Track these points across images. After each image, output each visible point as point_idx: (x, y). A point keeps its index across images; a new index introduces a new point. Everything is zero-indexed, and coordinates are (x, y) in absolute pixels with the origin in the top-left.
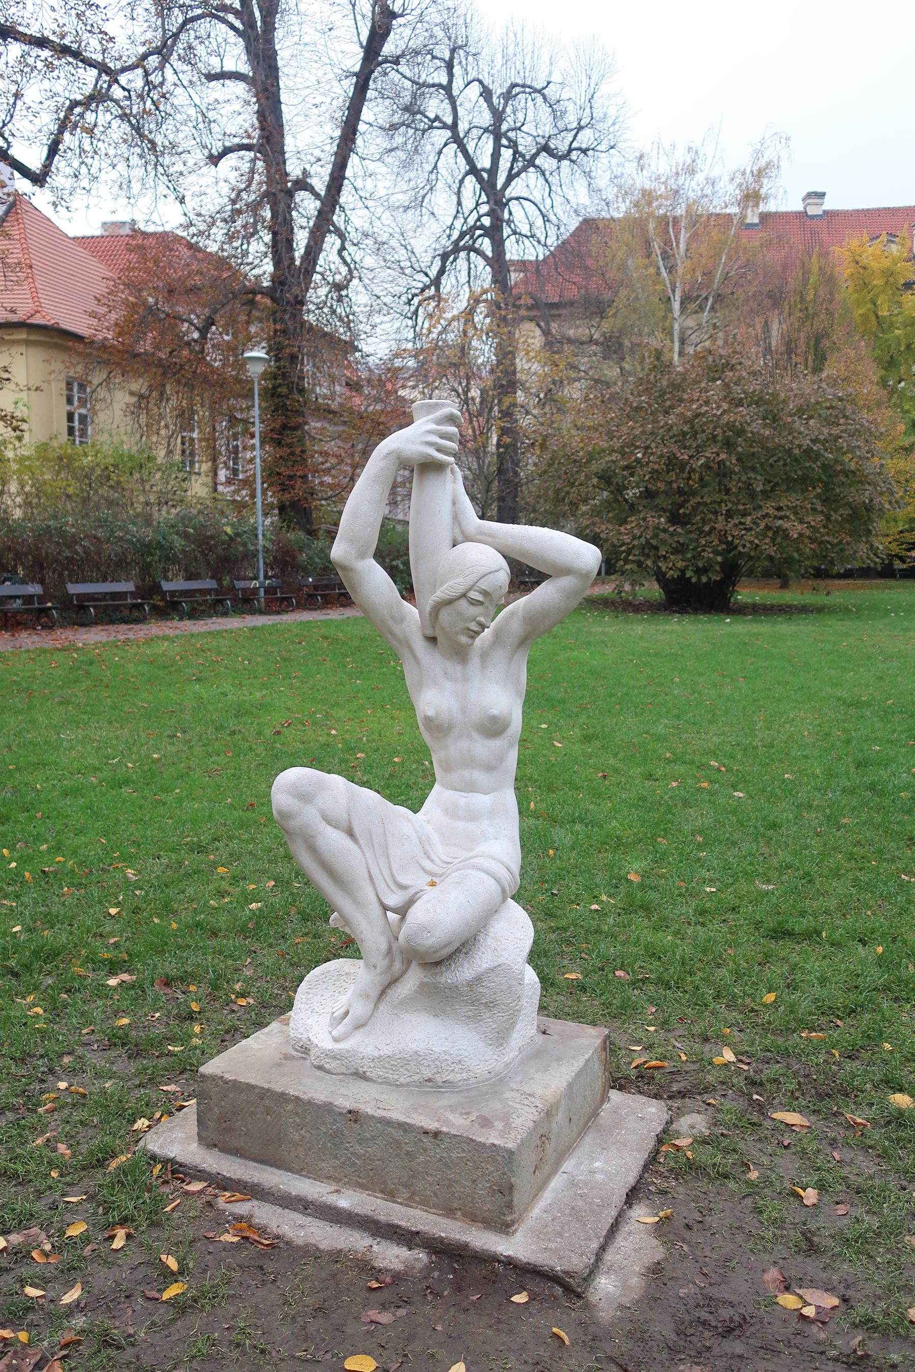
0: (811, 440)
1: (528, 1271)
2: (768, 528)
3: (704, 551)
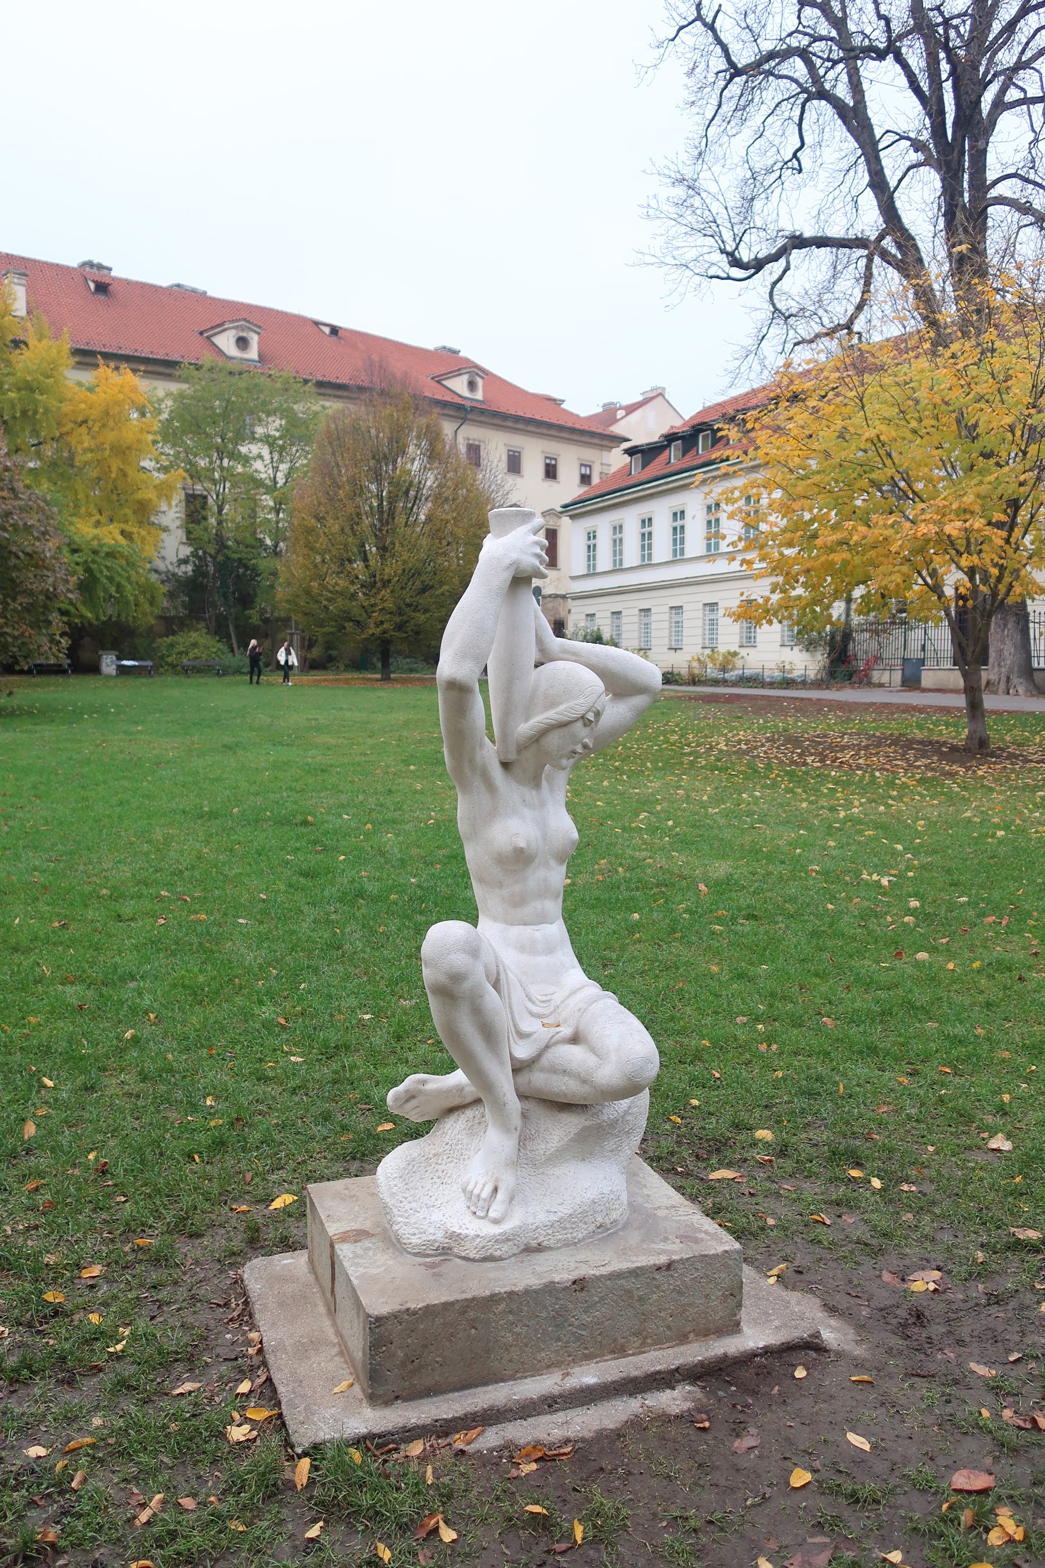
1: (783, 1351)
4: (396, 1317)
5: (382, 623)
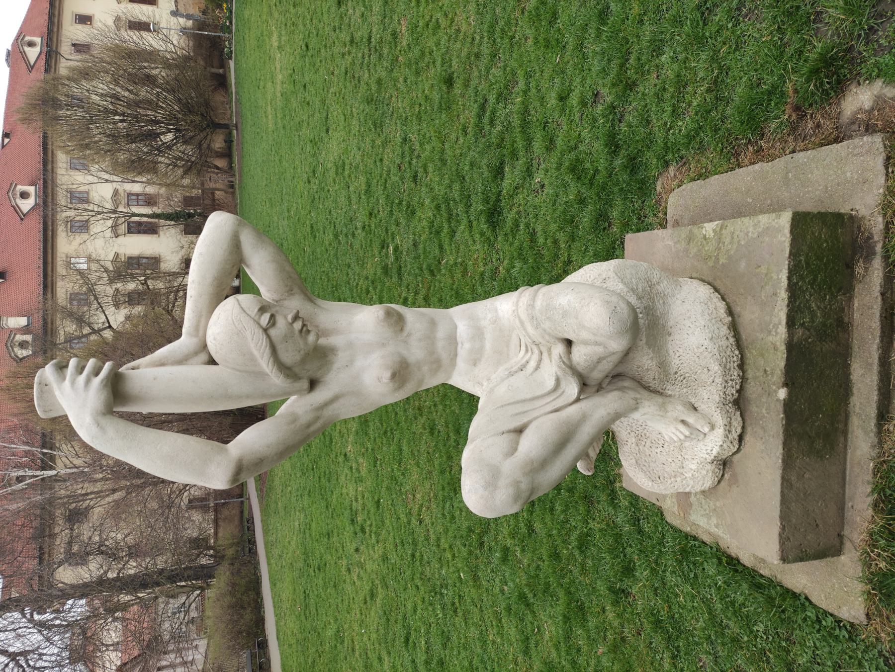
4: (784, 543)
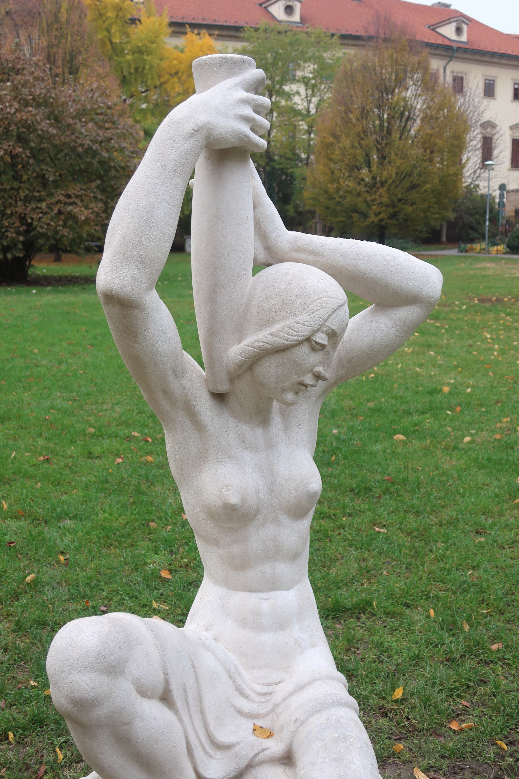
0: (91, 141)
2: (60, 212)
3: (6, 231)
5: (379, 213)
